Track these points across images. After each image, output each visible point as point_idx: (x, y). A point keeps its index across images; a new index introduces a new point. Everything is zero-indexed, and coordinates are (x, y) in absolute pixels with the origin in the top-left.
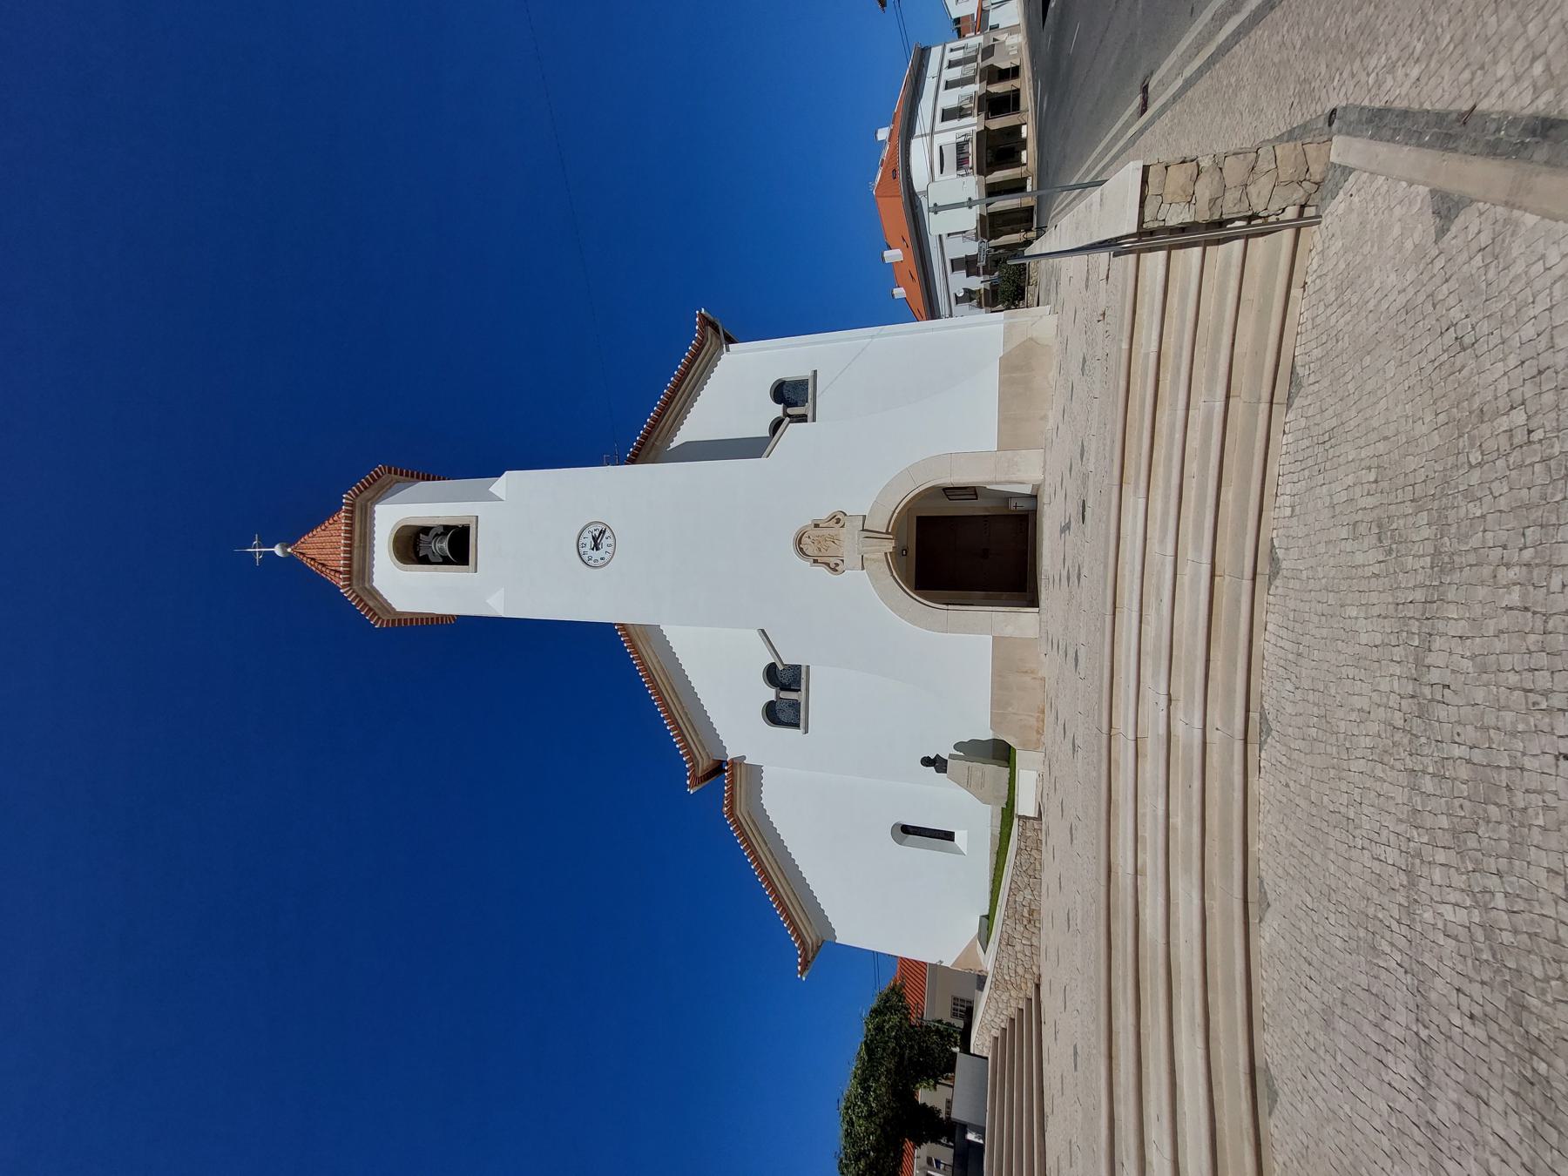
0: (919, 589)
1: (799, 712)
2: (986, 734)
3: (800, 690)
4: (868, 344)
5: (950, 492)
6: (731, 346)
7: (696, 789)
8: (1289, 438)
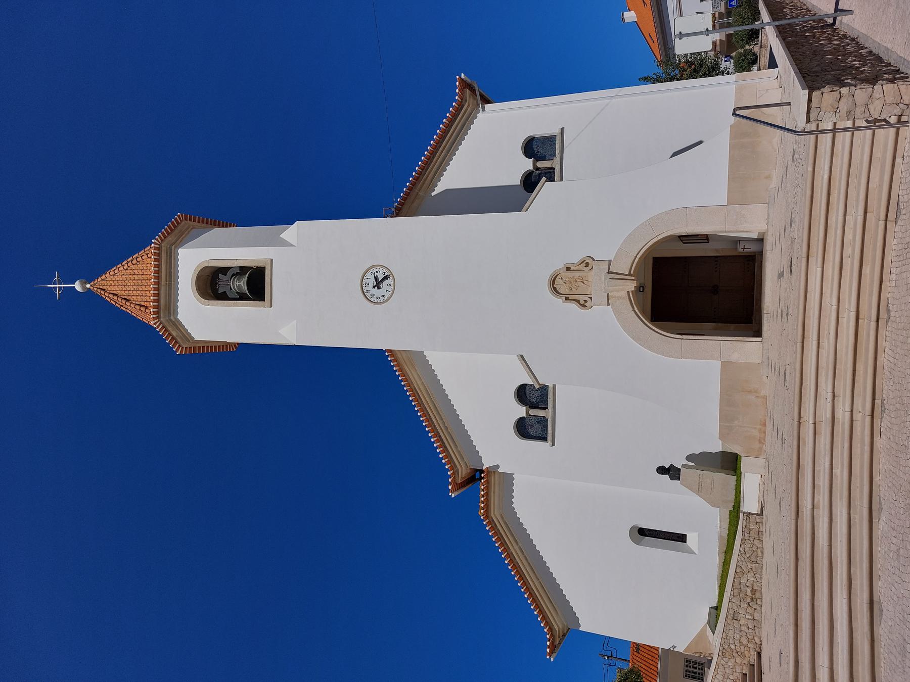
0: (653, 321)
1: (546, 427)
2: (715, 447)
3: (547, 408)
4: (607, 105)
5: (685, 239)
6: (486, 106)
7: (457, 493)
8: (895, 242)
